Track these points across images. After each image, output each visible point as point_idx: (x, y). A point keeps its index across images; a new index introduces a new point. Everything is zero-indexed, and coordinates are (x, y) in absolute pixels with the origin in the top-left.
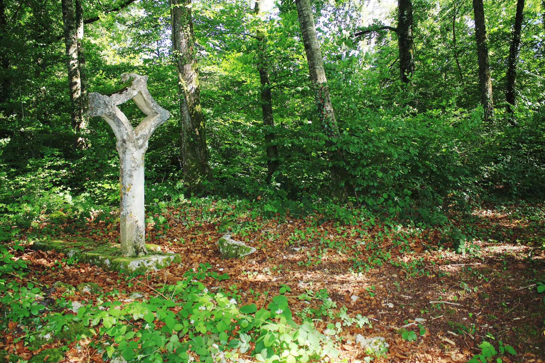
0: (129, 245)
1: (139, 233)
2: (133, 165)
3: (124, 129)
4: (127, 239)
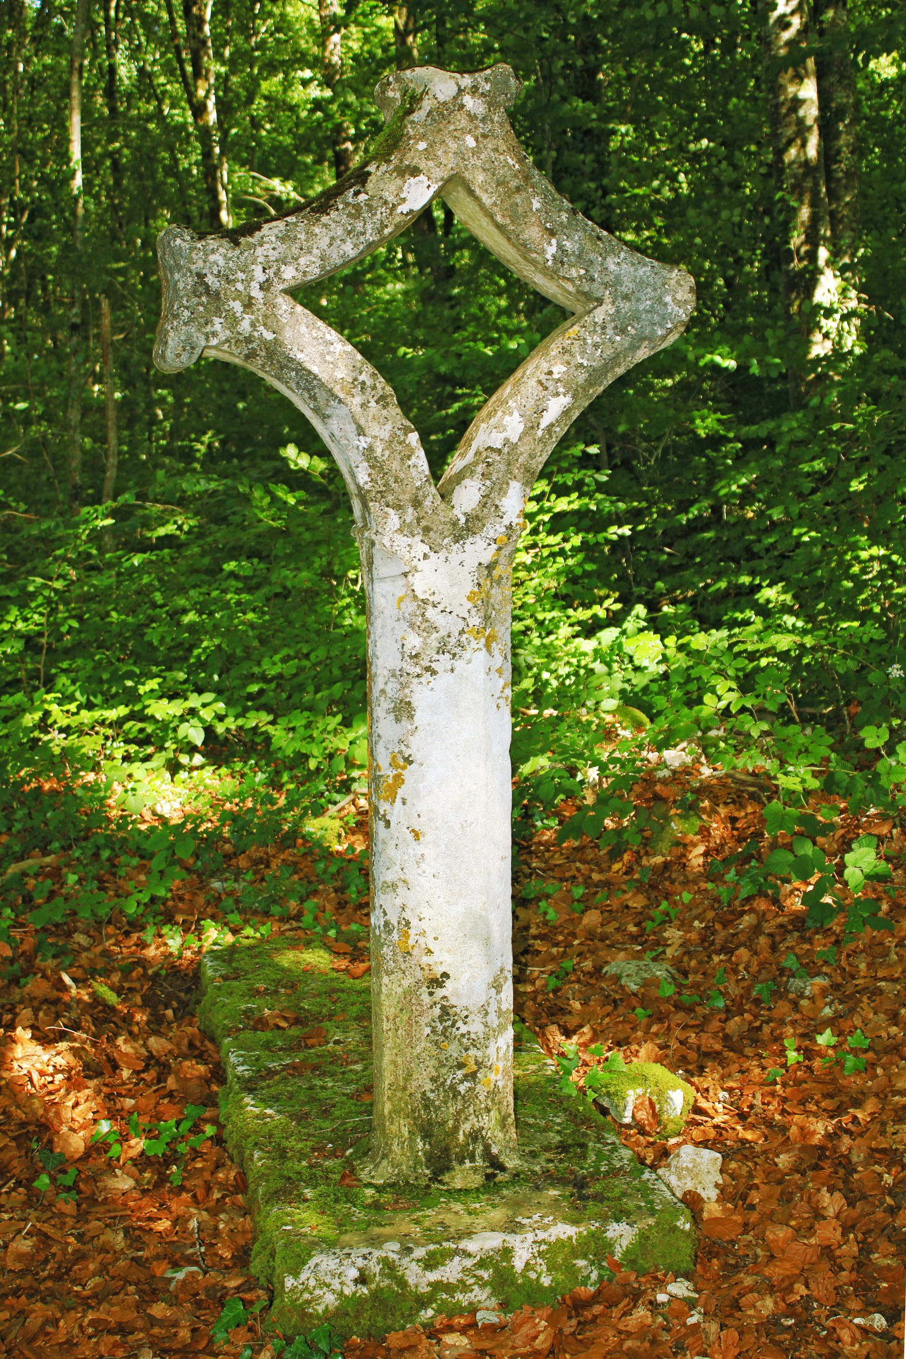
0: (396, 1111)
1: (453, 1050)
2: (414, 641)
3: (351, 428)
4: (388, 1079)
